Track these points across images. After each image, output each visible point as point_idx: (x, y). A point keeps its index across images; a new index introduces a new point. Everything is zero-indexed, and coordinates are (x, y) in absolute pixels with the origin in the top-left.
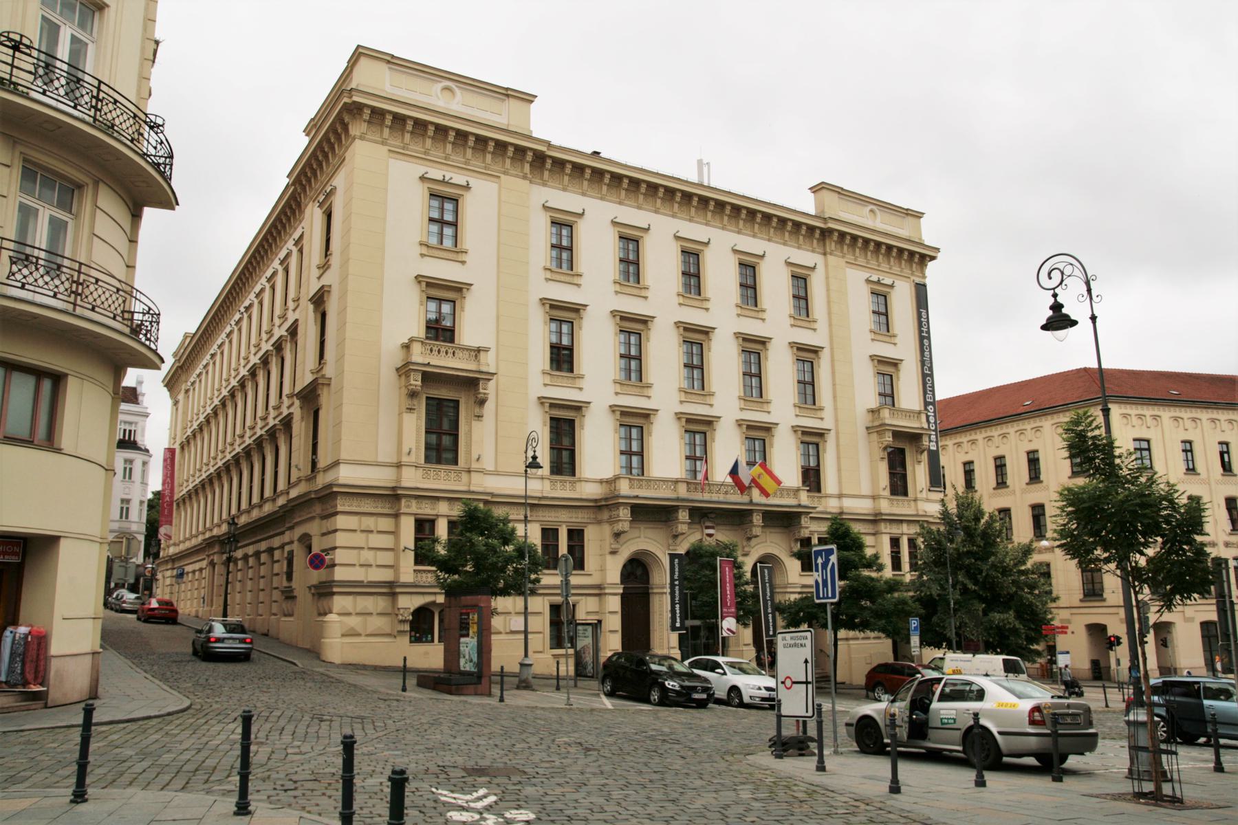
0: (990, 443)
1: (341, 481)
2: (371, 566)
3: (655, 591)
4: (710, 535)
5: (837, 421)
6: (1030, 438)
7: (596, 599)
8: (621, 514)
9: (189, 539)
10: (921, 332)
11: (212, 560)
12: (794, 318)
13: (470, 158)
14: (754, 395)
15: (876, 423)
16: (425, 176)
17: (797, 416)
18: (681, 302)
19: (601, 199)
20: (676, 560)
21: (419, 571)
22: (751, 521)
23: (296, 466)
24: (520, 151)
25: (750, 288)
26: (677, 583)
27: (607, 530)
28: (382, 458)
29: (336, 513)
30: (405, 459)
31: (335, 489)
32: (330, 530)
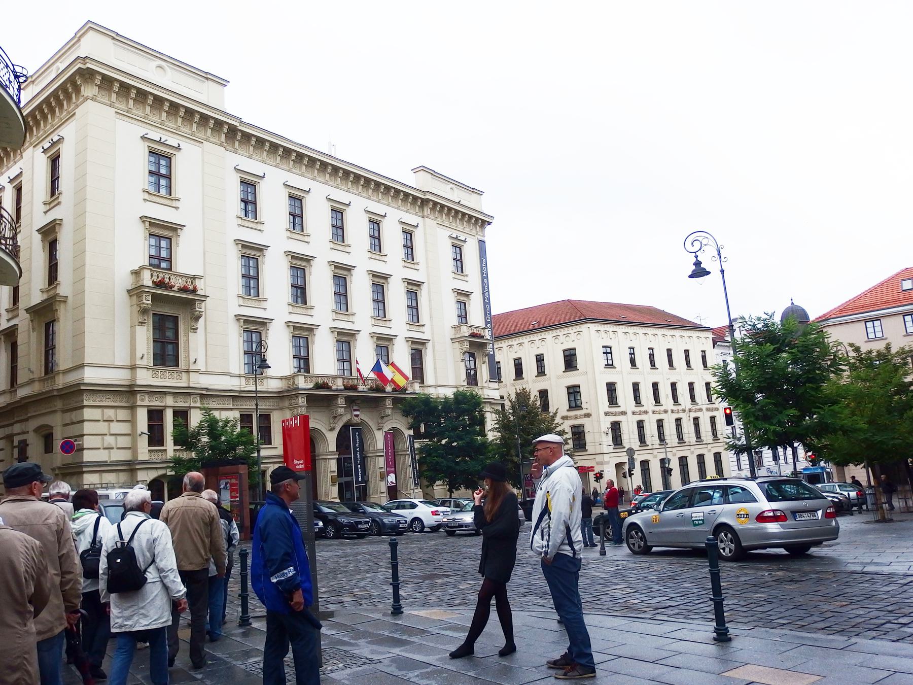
0: (511, 349)
1: (86, 381)
4: (357, 416)
5: (432, 334)
8: (300, 402)
13: (132, 107)
14: (252, 294)
15: (458, 336)
22: (385, 405)
24: (219, 124)
25: (297, 218)
28: (118, 363)
29: (83, 407)
30: (139, 362)
32: (75, 420)
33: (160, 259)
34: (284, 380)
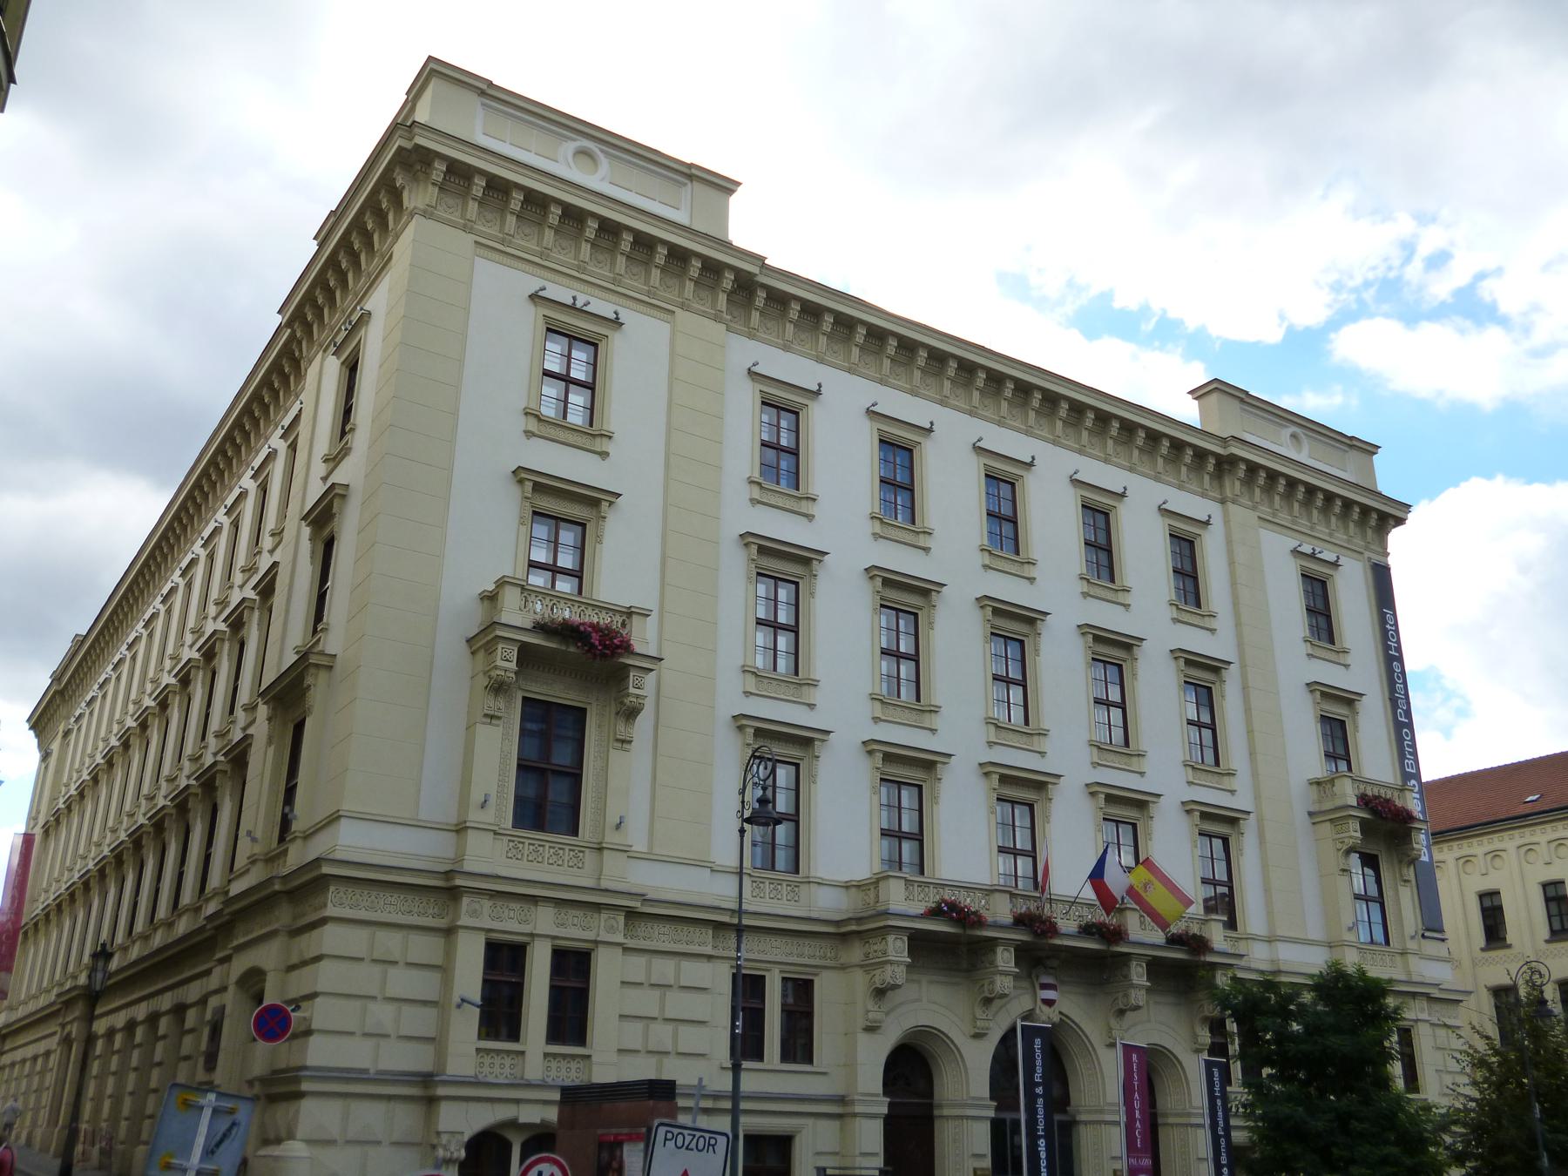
2: (387, 1036)
3: (946, 1112)
4: (1049, 1003)
5: (1257, 797)
6: (1548, 860)
7: (835, 1124)
8: (507, 1070)
9: (35, 997)
10: (1387, 648)
11: (69, 1034)
12: (1178, 608)
15: (1328, 806)
16: (541, 293)
17: (1190, 783)
18: (987, 562)
19: (850, 371)
20: (1038, 1041)
21: (488, 1051)
23: (249, 833)
24: (713, 269)
26: (1039, 1090)
27: (860, 981)
30: (475, 816)
31: (326, 870)
33: (554, 570)
34: (854, 890)
